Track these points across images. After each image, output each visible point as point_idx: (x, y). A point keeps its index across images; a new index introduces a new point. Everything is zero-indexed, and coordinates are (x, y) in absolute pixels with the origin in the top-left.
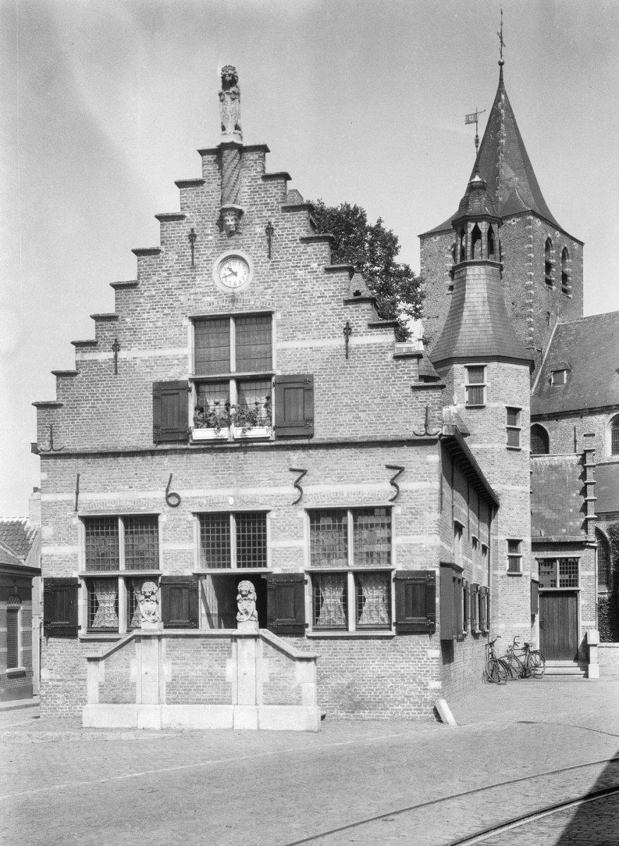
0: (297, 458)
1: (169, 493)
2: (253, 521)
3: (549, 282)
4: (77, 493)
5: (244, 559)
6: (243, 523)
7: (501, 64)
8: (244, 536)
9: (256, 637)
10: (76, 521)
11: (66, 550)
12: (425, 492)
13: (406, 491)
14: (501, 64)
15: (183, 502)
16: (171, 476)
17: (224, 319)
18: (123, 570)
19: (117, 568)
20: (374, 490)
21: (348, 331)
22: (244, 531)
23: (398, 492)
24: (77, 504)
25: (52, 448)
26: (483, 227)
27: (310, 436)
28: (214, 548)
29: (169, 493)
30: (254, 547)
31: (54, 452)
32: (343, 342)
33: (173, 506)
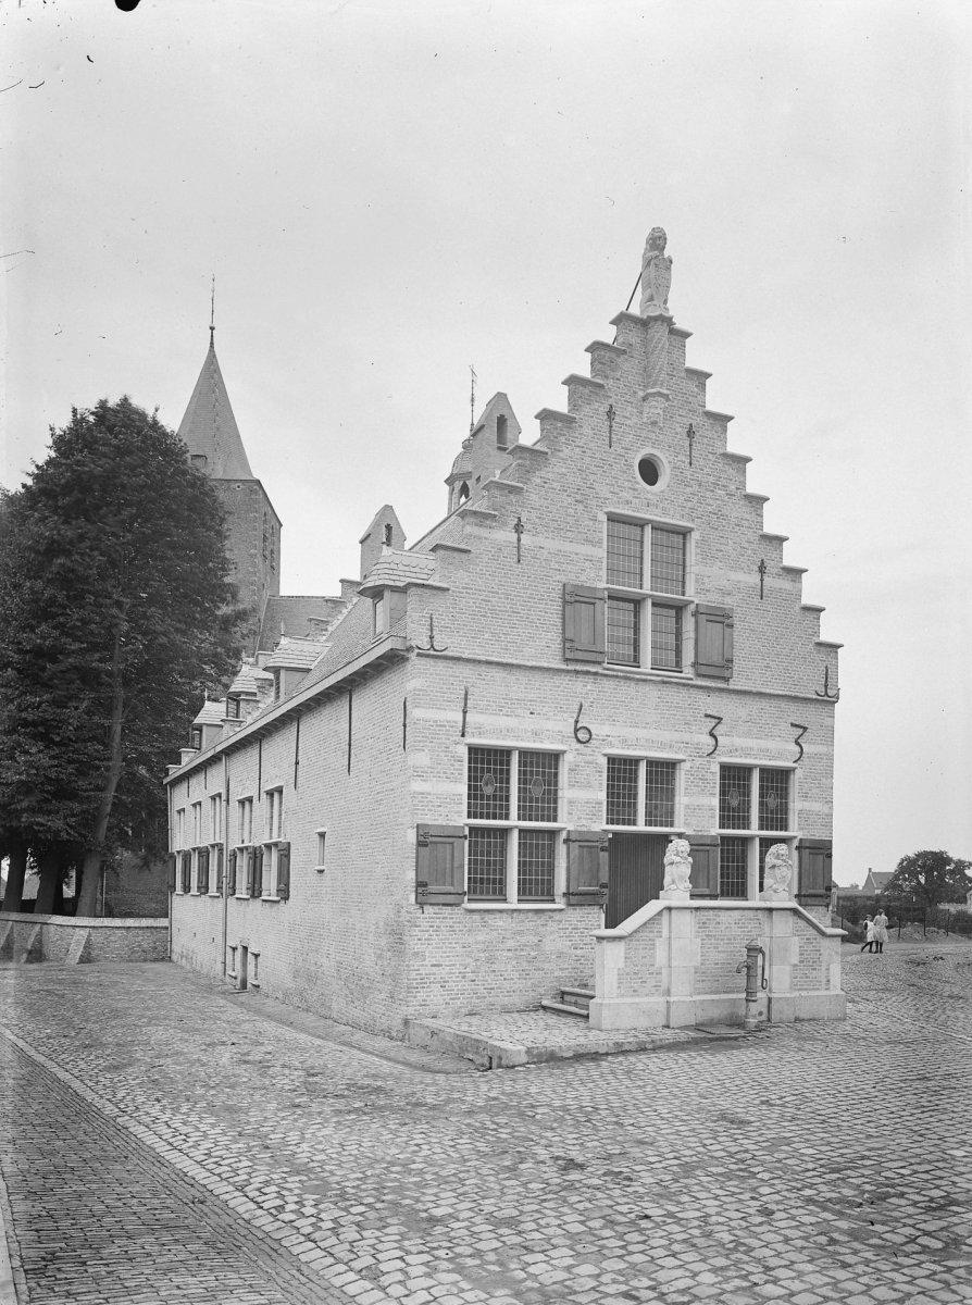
0: (714, 704)
1: (579, 725)
4: (465, 712)
7: (212, 329)
9: (794, 911)
14: (212, 329)
16: (581, 706)
18: (754, 830)
21: (762, 569)
23: (576, 735)
24: (464, 726)
25: (432, 646)
27: (727, 680)
29: (579, 725)
31: (435, 653)
32: (758, 581)
33: (579, 741)
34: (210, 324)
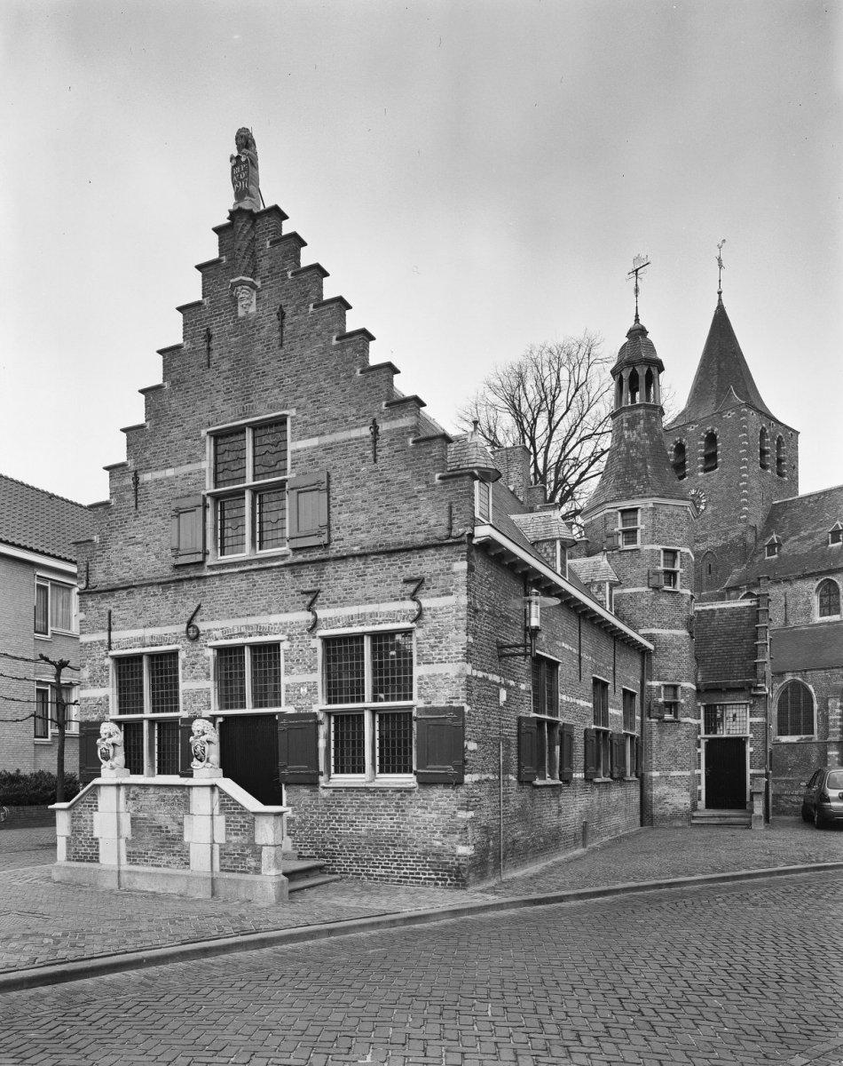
2: (267, 654)
3: (764, 467)
5: (335, 693)
6: (255, 652)
7: (720, 293)
8: (381, 663)
10: (108, 662)
11: (96, 693)
12: (451, 609)
13: (429, 609)
14: (720, 293)
15: (202, 635)
16: (199, 607)
17: (240, 430)
19: (141, 711)
20: (388, 613)
22: (380, 657)
26: (642, 371)
28: (340, 682)
30: (268, 688)
34: (717, 289)
